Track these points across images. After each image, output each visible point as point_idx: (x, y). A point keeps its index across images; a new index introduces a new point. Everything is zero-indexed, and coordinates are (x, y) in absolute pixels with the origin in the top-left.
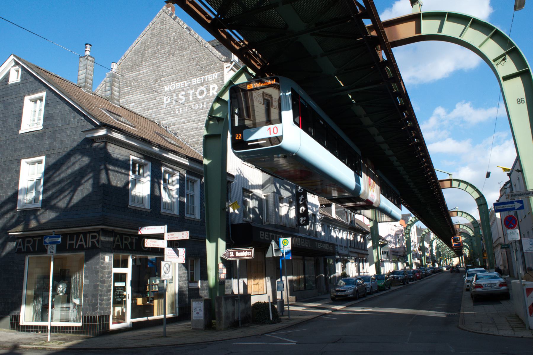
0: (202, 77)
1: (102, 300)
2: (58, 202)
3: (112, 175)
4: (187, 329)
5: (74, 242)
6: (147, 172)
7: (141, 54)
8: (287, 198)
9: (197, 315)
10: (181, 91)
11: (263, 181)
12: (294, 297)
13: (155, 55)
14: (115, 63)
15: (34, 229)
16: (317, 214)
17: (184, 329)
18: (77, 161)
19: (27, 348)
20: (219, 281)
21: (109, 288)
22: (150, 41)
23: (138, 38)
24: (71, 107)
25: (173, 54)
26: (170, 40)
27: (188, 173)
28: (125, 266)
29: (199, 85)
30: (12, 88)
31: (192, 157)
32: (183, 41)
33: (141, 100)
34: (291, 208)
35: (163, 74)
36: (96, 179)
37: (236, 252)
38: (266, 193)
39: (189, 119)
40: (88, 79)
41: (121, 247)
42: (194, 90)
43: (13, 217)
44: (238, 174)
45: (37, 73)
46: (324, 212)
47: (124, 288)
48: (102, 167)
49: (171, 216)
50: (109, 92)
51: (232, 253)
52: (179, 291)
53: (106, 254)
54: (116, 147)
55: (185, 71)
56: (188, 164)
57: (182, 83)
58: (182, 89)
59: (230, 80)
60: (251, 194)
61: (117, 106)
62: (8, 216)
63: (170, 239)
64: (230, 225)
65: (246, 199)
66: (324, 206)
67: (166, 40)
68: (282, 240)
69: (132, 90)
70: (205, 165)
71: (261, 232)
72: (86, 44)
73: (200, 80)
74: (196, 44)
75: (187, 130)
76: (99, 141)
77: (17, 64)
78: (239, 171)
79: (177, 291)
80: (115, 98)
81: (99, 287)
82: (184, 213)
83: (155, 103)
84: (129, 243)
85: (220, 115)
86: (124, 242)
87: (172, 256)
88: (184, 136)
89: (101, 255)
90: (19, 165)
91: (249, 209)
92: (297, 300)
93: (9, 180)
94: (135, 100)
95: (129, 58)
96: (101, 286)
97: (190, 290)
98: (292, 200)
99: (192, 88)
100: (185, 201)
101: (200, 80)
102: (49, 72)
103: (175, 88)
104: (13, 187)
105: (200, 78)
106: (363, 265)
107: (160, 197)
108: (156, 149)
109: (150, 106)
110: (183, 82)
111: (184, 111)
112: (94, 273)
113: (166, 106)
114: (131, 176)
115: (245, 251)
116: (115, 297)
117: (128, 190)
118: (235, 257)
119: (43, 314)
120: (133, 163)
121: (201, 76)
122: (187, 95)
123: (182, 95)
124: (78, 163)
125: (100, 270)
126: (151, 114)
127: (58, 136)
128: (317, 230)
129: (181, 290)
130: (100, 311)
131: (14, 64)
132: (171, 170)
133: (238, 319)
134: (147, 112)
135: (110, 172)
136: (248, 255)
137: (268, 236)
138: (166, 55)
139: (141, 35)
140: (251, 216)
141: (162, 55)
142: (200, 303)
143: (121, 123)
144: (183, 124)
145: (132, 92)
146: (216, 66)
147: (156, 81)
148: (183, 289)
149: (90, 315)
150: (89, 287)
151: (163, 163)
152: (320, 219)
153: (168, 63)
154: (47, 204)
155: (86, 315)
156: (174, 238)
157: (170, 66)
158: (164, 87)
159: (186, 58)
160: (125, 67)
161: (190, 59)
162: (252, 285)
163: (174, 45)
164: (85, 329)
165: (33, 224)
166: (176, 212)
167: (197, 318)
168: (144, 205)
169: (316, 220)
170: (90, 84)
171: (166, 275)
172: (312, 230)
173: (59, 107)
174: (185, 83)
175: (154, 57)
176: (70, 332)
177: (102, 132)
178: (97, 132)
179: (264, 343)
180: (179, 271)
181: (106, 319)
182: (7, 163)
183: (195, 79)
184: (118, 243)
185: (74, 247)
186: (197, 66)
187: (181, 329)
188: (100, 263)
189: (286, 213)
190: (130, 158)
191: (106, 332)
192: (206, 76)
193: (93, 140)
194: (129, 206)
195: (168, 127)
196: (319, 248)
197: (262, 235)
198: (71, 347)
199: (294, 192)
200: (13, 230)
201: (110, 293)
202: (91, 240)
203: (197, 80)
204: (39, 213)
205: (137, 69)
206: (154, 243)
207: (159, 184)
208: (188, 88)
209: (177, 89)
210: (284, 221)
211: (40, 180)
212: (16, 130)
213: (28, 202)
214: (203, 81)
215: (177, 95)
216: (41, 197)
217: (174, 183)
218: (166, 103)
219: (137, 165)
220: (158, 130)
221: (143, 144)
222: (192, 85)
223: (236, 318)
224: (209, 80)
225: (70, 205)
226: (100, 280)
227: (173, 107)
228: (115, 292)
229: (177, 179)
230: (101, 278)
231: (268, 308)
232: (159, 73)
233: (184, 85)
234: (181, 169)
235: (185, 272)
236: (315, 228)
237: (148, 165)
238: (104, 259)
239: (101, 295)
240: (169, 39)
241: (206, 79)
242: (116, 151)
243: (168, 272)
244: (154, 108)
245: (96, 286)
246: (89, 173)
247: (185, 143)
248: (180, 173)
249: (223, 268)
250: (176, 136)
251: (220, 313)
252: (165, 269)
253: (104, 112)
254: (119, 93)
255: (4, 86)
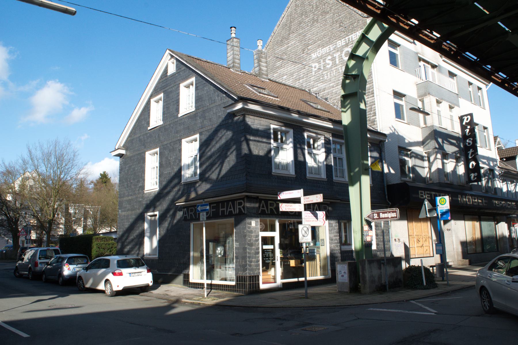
0: (346, 38)
1: (251, 262)
2: (211, 174)
3: (254, 145)
4: (334, 291)
5: (225, 209)
6: (289, 139)
7: (288, 28)
8: (453, 153)
9: (342, 278)
10: (328, 55)
11: (422, 137)
12: (467, 260)
13: (301, 26)
14: (260, 40)
15: (193, 199)
16: (495, 169)
17: (331, 292)
18: (223, 136)
19: (187, 303)
20: (365, 244)
21: (257, 251)
22: (295, 13)
23: (284, 13)
24: (214, 87)
25: (317, 21)
26: (312, 8)
27: (334, 136)
28: (273, 229)
29: (344, 47)
30: (171, 78)
31: (336, 119)
32: (325, 6)
33: (292, 71)
34: (459, 164)
35: (310, 42)
36: (239, 150)
37: (381, 214)
38: (427, 150)
39: (338, 82)
40: (236, 59)
41: (267, 212)
42: (339, 52)
43: (179, 190)
44: (391, 132)
45: (186, 61)
46: (507, 166)
47: (273, 251)
48: (243, 139)
49: (318, 180)
50: (257, 69)
51: (376, 215)
52: (331, 253)
53: (252, 219)
54: (255, 118)
55: (330, 35)
56: (332, 127)
57: (328, 48)
58: (328, 54)
59: (363, 34)
60: (409, 153)
61: (266, 80)
62: (176, 189)
63: (306, 203)
64: (386, 185)
65: (403, 157)
66: (505, 159)
67: (308, 8)
68: (438, 199)
69: (283, 63)
70: (344, 126)
71: (420, 192)
72: (231, 28)
73: (345, 41)
74: (337, 6)
75: (336, 94)
76: (239, 115)
77: (172, 57)
78: (393, 129)
79: (328, 254)
80: (263, 73)
81: (247, 250)
82: (333, 177)
83: (305, 72)
84: (274, 208)
85: (355, 72)
86: (269, 207)
87: (310, 220)
88: (334, 100)
89: (248, 220)
90: (180, 144)
91: (409, 168)
92: (470, 263)
93: (175, 158)
94: (287, 72)
95: (278, 33)
96: (249, 249)
97: (342, 252)
98: (460, 155)
99: (338, 51)
100: (333, 165)
101: (345, 41)
102: (200, 59)
103: (322, 53)
104: (178, 164)
105: (344, 39)
106: (454, 162)
107: (305, 163)
108: (295, 116)
109: (301, 76)
110: (329, 47)
111: (332, 75)
112: (243, 238)
113: (315, 73)
114: (273, 144)
115: (389, 212)
116: (264, 259)
117: (271, 158)
118: (380, 218)
119: (210, 273)
120: (274, 131)
121: (345, 37)
122: (333, 59)
123: (329, 60)
124: (224, 137)
125: (248, 234)
126: (302, 83)
127: (207, 114)
128: (497, 187)
129: (333, 252)
130: (249, 272)
131: (170, 57)
132: (314, 135)
133: (385, 283)
134: (298, 82)
135: (251, 142)
136: (393, 216)
137: (429, 196)
138: (310, 23)
139: (287, 9)
140: (411, 175)
141: (306, 24)
142: (344, 265)
143: (263, 95)
144: (332, 89)
145: (284, 65)
146: (359, 24)
147: (304, 50)
148: (335, 252)
149: (241, 275)
150: (239, 250)
151: (306, 128)
152: (500, 174)
153: (313, 30)
154: (203, 177)
155: (238, 275)
156: (309, 201)
157: (315, 33)
158: (311, 55)
159: (330, 21)
160: (275, 43)
161: (333, 22)
162: (416, 248)
163: (317, 12)
164: (238, 288)
165: (193, 195)
166: (323, 176)
167: (342, 281)
168: (289, 171)
169: (494, 176)
170: (238, 64)
171: (304, 238)
172: (490, 187)
173: (205, 89)
174: (331, 47)
175: (300, 27)
176: (227, 290)
177: (239, 106)
178: (235, 107)
179: (400, 311)
180: (329, 233)
181: (256, 279)
182: (172, 144)
183: (340, 41)
184: (230, 210)
185: (225, 214)
186: (341, 28)
187: (328, 291)
188: (247, 228)
189: (452, 169)
190: (270, 127)
191: (255, 290)
192: (350, 36)
193: (233, 114)
194: (272, 173)
195: (318, 94)
196: (498, 206)
197: (422, 195)
198: (219, 303)
199: (462, 146)
200: (179, 201)
201: (258, 255)
202: (238, 207)
203: (341, 42)
204: (197, 185)
205: (286, 42)
206: (289, 207)
207: (303, 150)
208: (334, 51)
209: (324, 55)
210: (451, 178)
211: (197, 155)
212: (176, 114)
213: (190, 176)
214: (347, 42)
215: (324, 61)
216: (198, 172)
217: (319, 148)
218: (314, 70)
219: (279, 133)
220: (307, 98)
221: (282, 113)
222: (338, 48)
223: (383, 282)
224: (353, 39)
225: (221, 176)
226: (248, 244)
227: (321, 73)
228: (264, 254)
229: (322, 143)
230: (249, 241)
231: (421, 273)
232: (306, 42)
233: (330, 49)
234: (326, 133)
235: (336, 234)
236: (493, 184)
237: (290, 132)
238: (250, 224)
239: (249, 257)
240: (312, 6)
241: (351, 39)
242: (256, 122)
243: (306, 235)
244: (305, 77)
245: (245, 249)
246: (233, 145)
247: (335, 107)
248: (325, 137)
249: (368, 231)
250: (326, 102)
251: (364, 276)
252: (303, 232)
253: (248, 87)
254: (267, 67)
255: (165, 78)
